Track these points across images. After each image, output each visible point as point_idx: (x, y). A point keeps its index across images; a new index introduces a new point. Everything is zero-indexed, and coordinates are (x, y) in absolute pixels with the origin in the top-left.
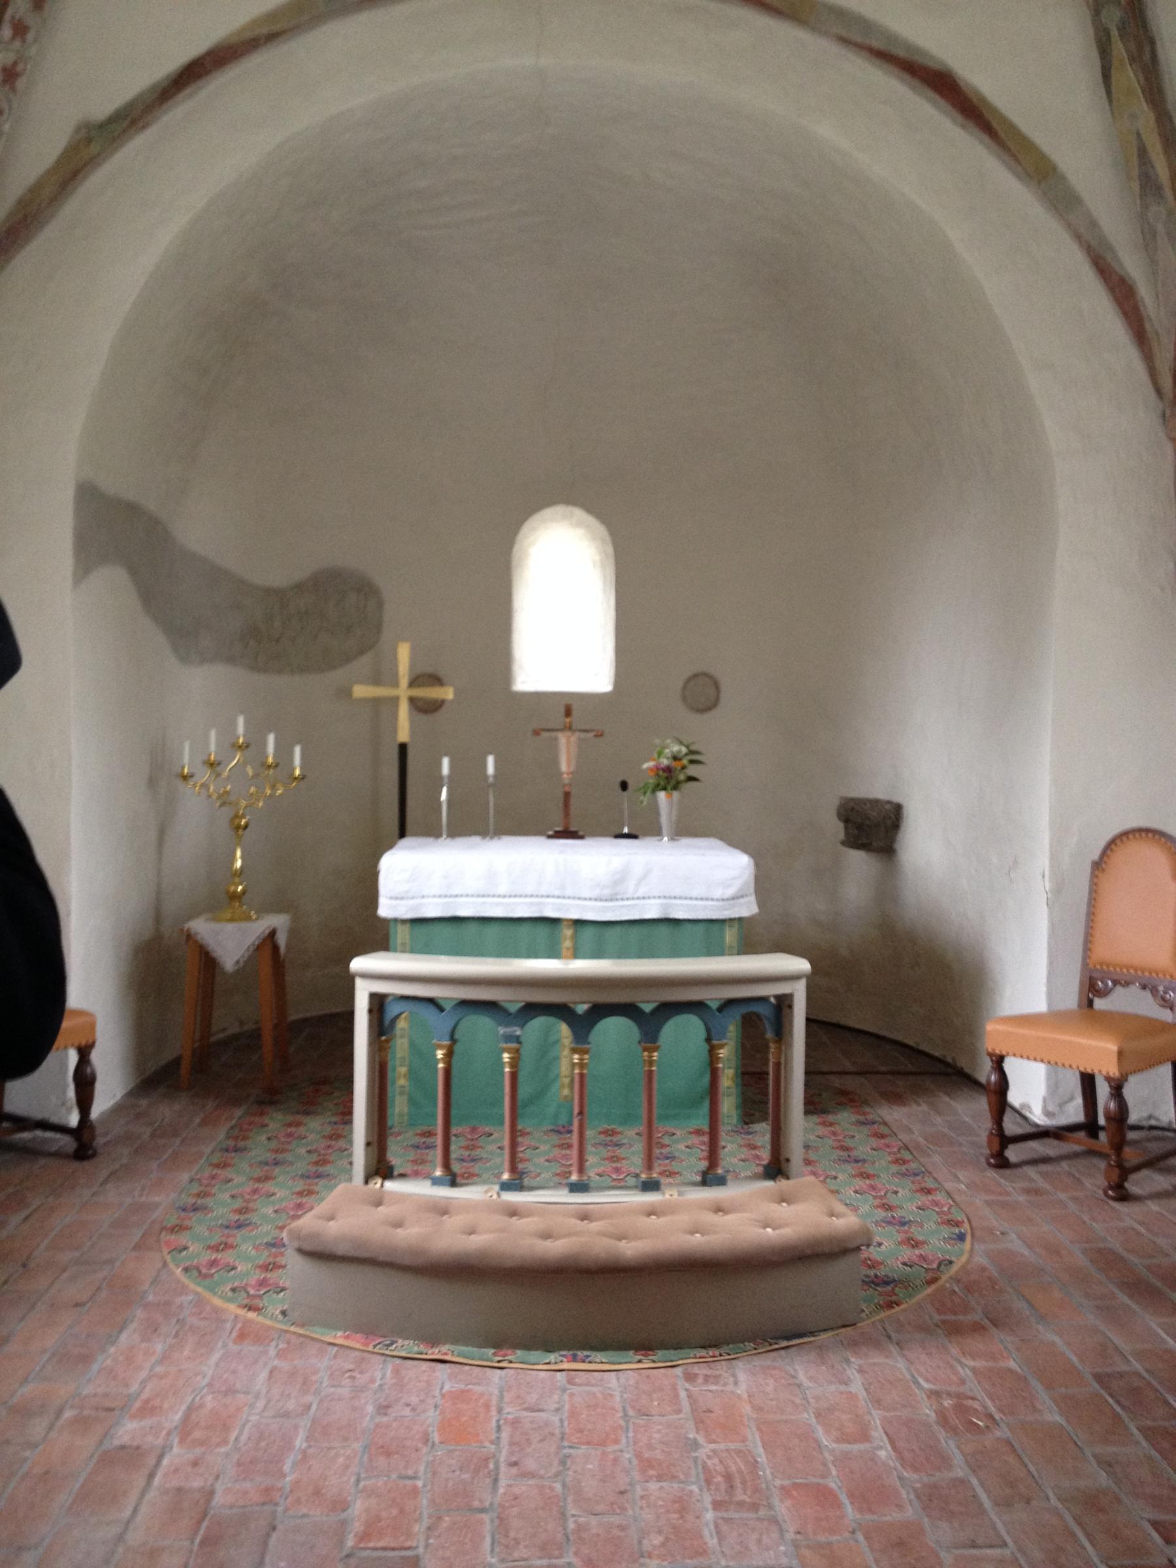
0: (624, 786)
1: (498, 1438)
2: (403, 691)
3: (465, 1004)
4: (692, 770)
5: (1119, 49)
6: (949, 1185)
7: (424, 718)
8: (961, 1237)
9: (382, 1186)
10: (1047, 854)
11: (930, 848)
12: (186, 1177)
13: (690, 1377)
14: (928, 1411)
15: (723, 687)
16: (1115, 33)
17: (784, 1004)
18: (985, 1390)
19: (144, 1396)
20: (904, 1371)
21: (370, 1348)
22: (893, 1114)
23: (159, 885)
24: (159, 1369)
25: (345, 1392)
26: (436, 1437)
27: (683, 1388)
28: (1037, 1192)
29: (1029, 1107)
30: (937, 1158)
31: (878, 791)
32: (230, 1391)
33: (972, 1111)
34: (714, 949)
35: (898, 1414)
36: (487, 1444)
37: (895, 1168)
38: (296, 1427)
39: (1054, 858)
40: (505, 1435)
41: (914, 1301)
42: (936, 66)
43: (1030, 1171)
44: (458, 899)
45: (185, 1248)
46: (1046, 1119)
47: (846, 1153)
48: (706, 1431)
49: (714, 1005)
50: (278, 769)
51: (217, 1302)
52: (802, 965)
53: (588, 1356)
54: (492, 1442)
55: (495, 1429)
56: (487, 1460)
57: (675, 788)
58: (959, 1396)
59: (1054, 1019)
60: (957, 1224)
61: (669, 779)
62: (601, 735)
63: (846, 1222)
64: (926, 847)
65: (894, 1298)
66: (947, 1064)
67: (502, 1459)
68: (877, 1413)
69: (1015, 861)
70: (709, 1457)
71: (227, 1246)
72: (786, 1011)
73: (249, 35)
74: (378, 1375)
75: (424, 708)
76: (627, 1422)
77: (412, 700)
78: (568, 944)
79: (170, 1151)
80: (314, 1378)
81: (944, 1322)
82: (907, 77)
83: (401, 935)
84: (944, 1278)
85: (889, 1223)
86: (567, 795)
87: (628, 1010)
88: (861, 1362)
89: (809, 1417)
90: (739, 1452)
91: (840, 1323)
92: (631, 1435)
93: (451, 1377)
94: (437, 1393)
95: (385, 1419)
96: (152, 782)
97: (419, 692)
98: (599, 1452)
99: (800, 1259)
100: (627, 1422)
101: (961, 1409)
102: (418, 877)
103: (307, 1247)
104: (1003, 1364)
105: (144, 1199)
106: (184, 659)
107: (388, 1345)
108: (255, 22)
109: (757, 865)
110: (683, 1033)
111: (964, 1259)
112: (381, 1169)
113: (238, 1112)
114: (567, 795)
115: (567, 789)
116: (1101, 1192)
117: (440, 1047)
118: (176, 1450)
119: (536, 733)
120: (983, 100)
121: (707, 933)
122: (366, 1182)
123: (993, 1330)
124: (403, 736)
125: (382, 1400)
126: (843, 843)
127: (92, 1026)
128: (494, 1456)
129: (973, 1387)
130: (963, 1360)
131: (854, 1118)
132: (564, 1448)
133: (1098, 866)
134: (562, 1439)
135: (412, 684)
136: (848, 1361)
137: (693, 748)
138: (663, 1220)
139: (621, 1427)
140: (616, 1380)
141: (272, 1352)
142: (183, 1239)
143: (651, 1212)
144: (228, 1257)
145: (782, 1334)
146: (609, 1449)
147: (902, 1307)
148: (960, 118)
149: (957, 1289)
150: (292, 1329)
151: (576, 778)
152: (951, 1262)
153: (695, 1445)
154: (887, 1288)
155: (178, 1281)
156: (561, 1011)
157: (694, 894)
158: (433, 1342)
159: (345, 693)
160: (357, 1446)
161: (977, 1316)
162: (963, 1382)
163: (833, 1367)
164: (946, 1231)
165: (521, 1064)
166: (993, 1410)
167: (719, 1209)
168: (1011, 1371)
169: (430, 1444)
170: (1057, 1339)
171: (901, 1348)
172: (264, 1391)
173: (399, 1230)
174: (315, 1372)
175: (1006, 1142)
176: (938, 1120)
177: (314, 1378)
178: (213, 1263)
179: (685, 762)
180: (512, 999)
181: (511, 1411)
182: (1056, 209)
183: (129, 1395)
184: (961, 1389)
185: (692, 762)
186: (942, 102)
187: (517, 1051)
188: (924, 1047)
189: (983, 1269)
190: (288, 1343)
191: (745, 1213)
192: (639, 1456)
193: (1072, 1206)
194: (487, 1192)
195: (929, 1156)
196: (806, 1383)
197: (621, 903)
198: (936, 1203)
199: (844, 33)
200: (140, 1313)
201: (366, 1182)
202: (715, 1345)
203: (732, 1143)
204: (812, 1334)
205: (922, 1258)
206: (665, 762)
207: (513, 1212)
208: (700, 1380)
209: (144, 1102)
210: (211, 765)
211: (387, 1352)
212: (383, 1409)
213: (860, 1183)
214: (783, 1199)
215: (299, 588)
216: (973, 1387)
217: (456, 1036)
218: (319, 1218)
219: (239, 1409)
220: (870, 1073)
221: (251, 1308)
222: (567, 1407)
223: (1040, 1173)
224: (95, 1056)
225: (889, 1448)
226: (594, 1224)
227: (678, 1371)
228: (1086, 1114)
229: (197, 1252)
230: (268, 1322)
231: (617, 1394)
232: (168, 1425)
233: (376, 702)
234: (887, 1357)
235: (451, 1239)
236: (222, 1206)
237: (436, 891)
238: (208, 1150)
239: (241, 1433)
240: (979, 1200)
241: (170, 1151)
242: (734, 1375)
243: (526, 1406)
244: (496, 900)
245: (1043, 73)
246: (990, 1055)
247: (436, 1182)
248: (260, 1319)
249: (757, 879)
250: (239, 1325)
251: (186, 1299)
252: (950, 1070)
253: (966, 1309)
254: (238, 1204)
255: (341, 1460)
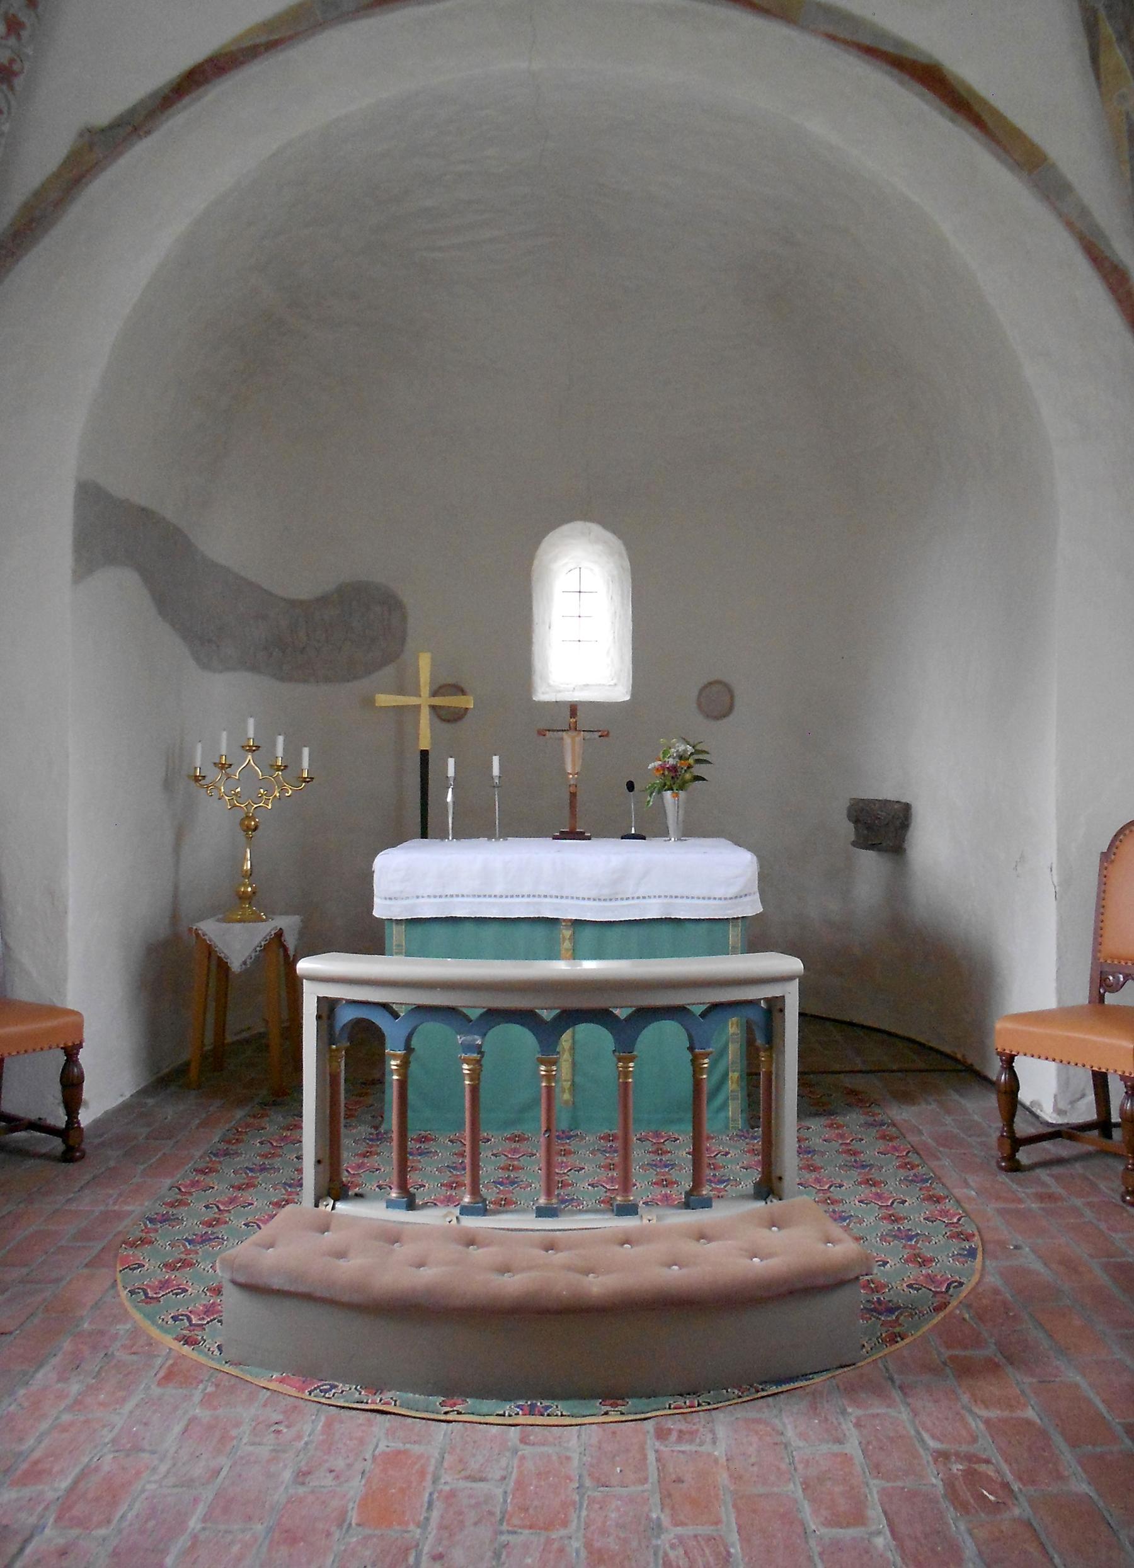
0: (631, 786)
1: (427, 1519)
2: (424, 699)
3: (419, 1008)
4: (699, 770)
5: (1107, 29)
6: (958, 1192)
7: (445, 726)
8: (972, 1253)
9: (333, 1208)
10: (1055, 847)
11: (937, 847)
12: (168, 1182)
13: (662, 1434)
14: (934, 1481)
15: (737, 693)
16: (1102, 13)
17: (775, 1007)
18: (999, 1449)
19: (37, 1454)
20: (908, 1425)
21: (306, 1395)
22: (901, 1114)
23: (176, 887)
24: (66, 1418)
25: (264, 1452)
26: (354, 1517)
27: (652, 1444)
28: (1051, 1197)
29: (1040, 1105)
30: (947, 1162)
31: (887, 791)
32: (137, 1449)
33: (982, 1108)
34: (718, 948)
35: (900, 1484)
36: (412, 1527)
37: (902, 1173)
38: (196, 1500)
39: (1061, 851)
40: (435, 1514)
41: (919, 1333)
42: (925, 61)
43: (1042, 1174)
44: (455, 900)
45: (141, 1266)
46: (1055, 1115)
47: (854, 1159)
48: (673, 1508)
49: (698, 1010)
50: (288, 771)
51: (155, 1332)
52: (795, 965)
53: (547, 1408)
54: (418, 1525)
55: (426, 1505)
56: (407, 1550)
57: (681, 788)
58: (970, 1458)
59: (1063, 1015)
60: (968, 1238)
61: (675, 777)
62: (607, 735)
63: (842, 1249)
64: (933, 845)
65: (897, 1330)
66: (956, 1060)
67: (426, 1549)
68: (874, 1482)
69: (1022, 857)
70: (673, 1547)
71: (187, 1264)
72: (776, 1014)
73: (247, 43)
74: (307, 1428)
75: (447, 717)
76: (582, 1497)
77: (434, 708)
78: (567, 945)
79: (160, 1155)
80: (234, 1433)
81: (953, 1358)
82: (896, 71)
83: (396, 936)
84: (954, 1303)
85: (895, 1237)
86: (573, 795)
87: (602, 1016)
88: (859, 1412)
89: (795, 1489)
90: (710, 1539)
91: (838, 1364)
92: (584, 1513)
93: (390, 1433)
94: (368, 1456)
95: (301, 1490)
96: (168, 785)
97: (439, 701)
98: (542, 1540)
99: (791, 1293)
100: (582, 1497)
101: (971, 1475)
102: (411, 878)
103: (242, 1279)
104: (1019, 1414)
105: (116, 1208)
106: (205, 666)
107: (326, 1391)
108: (250, 32)
109: (761, 866)
110: (664, 1040)
111: (975, 1278)
112: (335, 1188)
113: (239, 1114)
114: (573, 795)
115: (572, 789)
116: (1118, 1198)
117: (395, 1057)
118: (47, 1531)
119: (541, 733)
120: (970, 90)
121: (709, 933)
122: (317, 1206)
123: (1009, 1369)
124: (424, 745)
125: (303, 1463)
126: (855, 844)
127: (79, 1027)
128: (417, 1545)
129: (986, 1446)
130: (976, 1410)
131: (862, 1119)
132: (502, 1533)
133: (1107, 857)
134: (501, 1521)
135: (434, 694)
136: (844, 1412)
137: (698, 748)
138: (639, 1249)
139: (574, 1503)
140: (575, 1440)
141: (197, 1396)
142: (139, 1254)
143: (626, 1240)
144: (181, 1277)
145: (766, 1379)
146: (554, 1535)
147: (906, 1341)
148: (948, 111)
149: (967, 1316)
150: (226, 1368)
151: (594, 780)
152: (961, 1284)
153: (658, 1528)
154: (889, 1316)
155: (122, 1305)
156: (526, 1017)
157: (696, 893)
158: (377, 1388)
159: (368, 702)
160: (259, 1528)
161: (990, 1351)
162: (974, 1439)
163: (826, 1419)
164: (955, 1246)
165: (484, 1074)
166: (1010, 1477)
167: (702, 1236)
168: (1029, 1423)
169: (345, 1526)
170: (1078, 1378)
171: (905, 1394)
172: (173, 1449)
173: (341, 1262)
174: (237, 1425)
175: (1017, 1145)
176: (948, 1120)
177: (234, 1433)
178: (164, 1284)
179: (691, 761)
180: (473, 1005)
181: (449, 1480)
182: (1048, 198)
183: (20, 1453)
184: (972, 1449)
185: (698, 761)
186: (930, 95)
187: (478, 1062)
188: (933, 1044)
189: (996, 1292)
190: (217, 1386)
191: (732, 1240)
192: (588, 1545)
193: (1089, 1214)
194: (445, 1216)
195: (938, 1159)
196: (796, 1442)
197: (619, 903)
198: (944, 1213)
199: (831, 29)
200: (67, 1345)
201: (317, 1206)
202: (694, 1393)
203: (736, 1148)
204: (805, 1376)
205: (931, 1278)
206: (671, 761)
207: (470, 1240)
208: (674, 1437)
209: (150, 1101)
210: (223, 767)
211: (323, 1400)
212: (302, 1476)
213: (865, 1191)
214: (773, 1222)
215: (323, 600)
216: (986, 1446)
217: (414, 1043)
218: (258, 1245)
219: (138, 1473)
220: (879, 1071)
221: (187, 1341)
222: (514, 1476)
223: (1052, 1176)
224: (83, 1057)
225: (888, 1533)
226: (560, 1255)
227: (649, 1426)
228: (1098, 1113)
229: (152, 1269)
230: (202, 1359)
231: (575, 1457)
232: (50, 1495)
233: (399, 710)
234: (889, 1406)
235: (397, 1274)
236: (191, 1221)
237: (430, 891)
238: (197, 1154)
239: (130, 1507)
240: (991, 1208)
241: (160, 1155)
242: (712, 1431)
243: (468, 1473)
244: (492, 900)
245: (1034, 69)
246: (1000, 1054)
247: (391, 1204)
248: (194, 1355)
249: (763, 877)
250: (170, 1362)
251: (122, 1328)
252: (960, 1067)
253: (977, 1341)
254: (212, 1214)
255: (235, 1549)
